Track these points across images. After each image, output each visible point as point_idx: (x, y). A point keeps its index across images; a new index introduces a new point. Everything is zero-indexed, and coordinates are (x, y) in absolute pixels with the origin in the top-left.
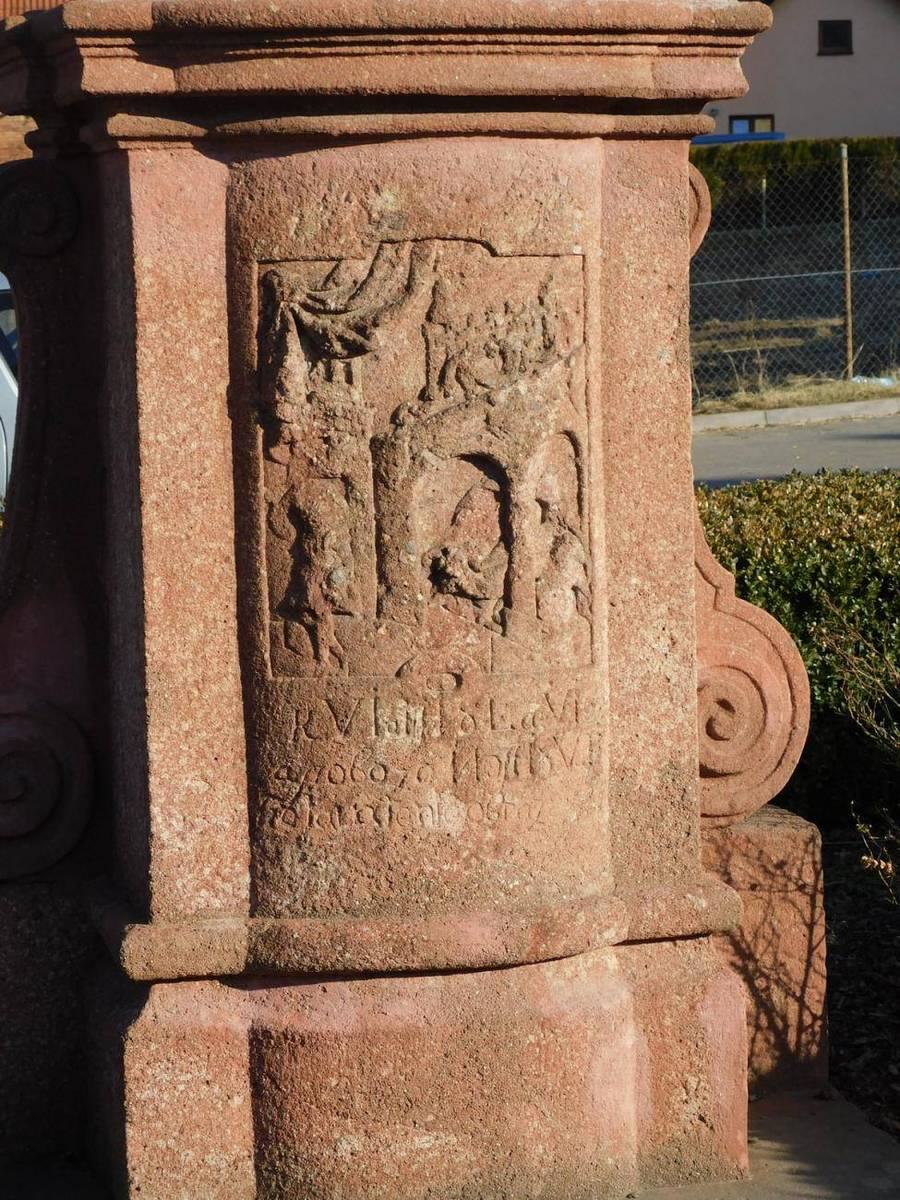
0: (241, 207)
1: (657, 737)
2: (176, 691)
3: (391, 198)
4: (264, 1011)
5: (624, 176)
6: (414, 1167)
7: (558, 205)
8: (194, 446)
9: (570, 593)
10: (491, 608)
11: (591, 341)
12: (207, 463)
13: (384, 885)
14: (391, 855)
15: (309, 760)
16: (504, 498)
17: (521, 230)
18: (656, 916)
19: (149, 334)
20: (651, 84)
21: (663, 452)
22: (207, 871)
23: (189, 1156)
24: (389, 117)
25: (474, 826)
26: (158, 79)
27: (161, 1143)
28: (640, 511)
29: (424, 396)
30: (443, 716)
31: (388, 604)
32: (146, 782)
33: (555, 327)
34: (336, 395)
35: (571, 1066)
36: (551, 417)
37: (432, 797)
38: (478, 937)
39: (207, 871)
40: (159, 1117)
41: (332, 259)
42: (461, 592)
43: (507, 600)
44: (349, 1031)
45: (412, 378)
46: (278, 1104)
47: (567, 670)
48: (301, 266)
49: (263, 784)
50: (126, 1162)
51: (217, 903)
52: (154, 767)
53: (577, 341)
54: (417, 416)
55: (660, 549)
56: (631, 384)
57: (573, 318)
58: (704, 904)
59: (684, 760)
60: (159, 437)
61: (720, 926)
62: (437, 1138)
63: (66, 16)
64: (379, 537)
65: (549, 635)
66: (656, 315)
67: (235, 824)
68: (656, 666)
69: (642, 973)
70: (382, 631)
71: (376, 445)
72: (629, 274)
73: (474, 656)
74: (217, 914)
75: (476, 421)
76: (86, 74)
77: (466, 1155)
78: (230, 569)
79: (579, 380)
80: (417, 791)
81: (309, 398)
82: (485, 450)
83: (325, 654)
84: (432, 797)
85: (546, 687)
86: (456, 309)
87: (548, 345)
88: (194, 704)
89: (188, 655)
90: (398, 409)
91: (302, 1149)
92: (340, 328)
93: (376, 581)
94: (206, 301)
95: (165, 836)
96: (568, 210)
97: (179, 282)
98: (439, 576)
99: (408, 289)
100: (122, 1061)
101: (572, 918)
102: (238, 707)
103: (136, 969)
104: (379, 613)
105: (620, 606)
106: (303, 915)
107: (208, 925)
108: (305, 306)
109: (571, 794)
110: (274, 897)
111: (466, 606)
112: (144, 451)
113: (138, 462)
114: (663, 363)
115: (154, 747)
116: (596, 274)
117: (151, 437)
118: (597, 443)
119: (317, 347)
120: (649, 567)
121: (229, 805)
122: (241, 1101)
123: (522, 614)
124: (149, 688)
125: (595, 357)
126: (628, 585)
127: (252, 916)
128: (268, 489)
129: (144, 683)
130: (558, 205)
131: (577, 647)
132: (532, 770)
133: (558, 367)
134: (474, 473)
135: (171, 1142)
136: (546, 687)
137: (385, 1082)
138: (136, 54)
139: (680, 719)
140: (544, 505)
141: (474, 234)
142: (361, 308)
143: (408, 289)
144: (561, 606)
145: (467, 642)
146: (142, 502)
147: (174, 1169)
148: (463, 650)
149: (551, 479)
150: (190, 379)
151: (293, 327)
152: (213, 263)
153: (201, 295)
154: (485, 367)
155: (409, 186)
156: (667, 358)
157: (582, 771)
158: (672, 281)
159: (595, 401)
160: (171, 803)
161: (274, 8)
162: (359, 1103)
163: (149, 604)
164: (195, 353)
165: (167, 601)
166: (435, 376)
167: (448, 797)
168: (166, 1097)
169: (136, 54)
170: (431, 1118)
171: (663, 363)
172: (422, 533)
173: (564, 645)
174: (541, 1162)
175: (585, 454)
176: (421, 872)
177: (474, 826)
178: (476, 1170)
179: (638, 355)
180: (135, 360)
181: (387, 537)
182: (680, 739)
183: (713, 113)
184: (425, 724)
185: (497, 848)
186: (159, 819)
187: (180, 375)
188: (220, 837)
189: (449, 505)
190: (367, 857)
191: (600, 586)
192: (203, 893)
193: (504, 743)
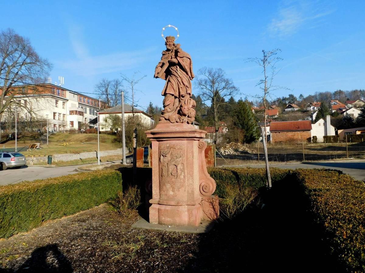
10: (176, 177)
18: (189, 203)
29: (171, 160)
37: (170, 191)
38: (173, 203)
45: (170, 159)
77: (172, 221)
84: (170, 191)
86: (173, 154)
99: (169, 152)
116: (186, 151)
121: (158, 191)
122: (157, 214)
123: (178, 177)
128: (160, 167)
142: (166, 153)
143: (169, 152)
145: (173, 179)
146: (335, 92)
152: (158, 150)
164: (156, 156)
165: (154, 175)
172: (170, 170)
173: (182, 180)
189: (173, 169)
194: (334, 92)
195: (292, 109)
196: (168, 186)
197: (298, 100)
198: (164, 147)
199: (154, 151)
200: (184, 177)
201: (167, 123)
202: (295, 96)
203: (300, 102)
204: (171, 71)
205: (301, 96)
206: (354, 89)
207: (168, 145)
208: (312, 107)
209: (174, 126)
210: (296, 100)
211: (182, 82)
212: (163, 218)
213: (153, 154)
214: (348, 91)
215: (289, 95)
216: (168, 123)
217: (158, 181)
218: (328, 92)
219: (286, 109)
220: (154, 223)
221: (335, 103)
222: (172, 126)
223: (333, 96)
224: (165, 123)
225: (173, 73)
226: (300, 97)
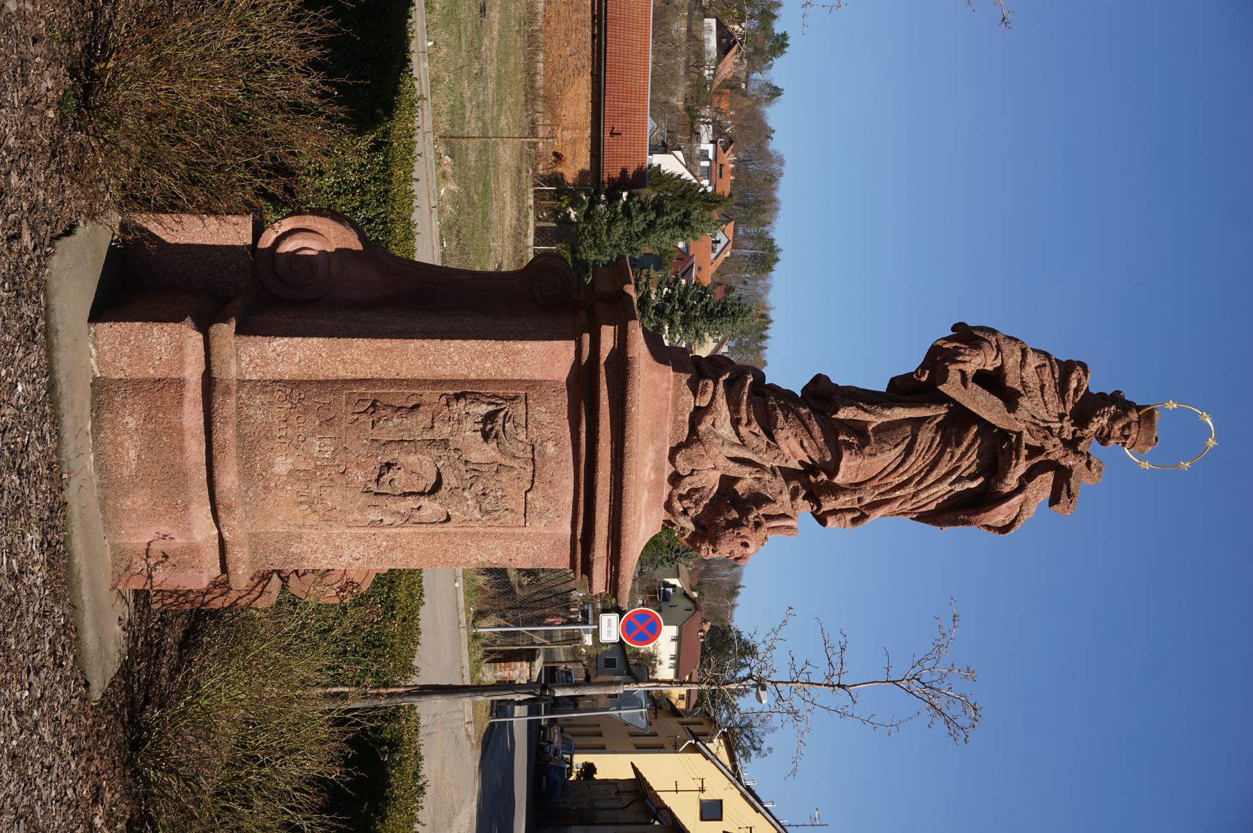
0: (549, 387)
1: (315, 552)
2: (340, 350)
3: (552, 450)
4: (194, 384)
5: (558, 543)
6: (120, 450)
7: (547, 517)
8: (448, 363)
9: (380, 518)
10: (374, 487)
11: (489, 528)
12: (440, 368)
13: (251, 439)
14: (264, 442)
15: (306, 409)
16: (422, 494)
17: (537, 503)
19: (498, 346)
20: (596, 556)
22: (258, 361)
23: (126, 349)
24: (584, 452)
25: (277, 478)
26: (604, 354)
27: (132, 338)
28: (415, 547)
29: (466, 462)
30: (326, 466)
31: (376, 444)
32: (298, 336)
33: (496, 515)
34: (468, 425)
35: (167, 517)
36: (457, 513)
37: (290, 460)
38: (228, 479)
39: (258, 361)
40: (144, 337)
41: (527, 425)
42: (381, 475)
43: (376, 494)
44: (184, 423)
45: (475, 457)
46: (152, 561)
47: (345, 517)
48: (524, 411)
49: (298, 387)
50: (124, 321)
51: (243, 364)
52: (306, 340)
53: (488, 523)
54: (459, 459)
55: (398, 555)
56: (470, 544)
57: (499, 522)
58: (240, 573)
59: (305, 563)
60: (452, 349)
61: (231, 579)
62: (134, 460)
63: (633, 321)
64: (406, 441)
65: (361, 510)
66: (499, 554)
67: (279, 374)
69: (209, 545)
70: (365, 441)
71: (445, 442)
72: (517, 544)
73: (353, 480)
74: (239, 363)
75: (454, 483)
76: (608, 327)
77: (126, 473)
78: (393, 375)
79: (471, 524)
80: (293, 454)
81: (467, 413)
82: (443, 486)
83: (356, 417)
84: (290, 460)
85: (338, 508)
87: (488, 512)
88: (333, 358)
89: (356, 357)
90: (924, 518)
91: (129, 401)
92: (497, 428)
93: (387, 439)
94: (510, 370)
95: (274, 344)
96: (545, 521)
97: (519, 359)
98: (389, 466)
99: (514, 456)
100: (171, 321)
101: (234, 519)
102: (332, 377)
103: (216, 329)
104: (373, 440)
105: (373, 538)
106: (237, 402)
107: (233, 361)
108: (507, 413)
109: (290, 517)
110: (245, 390)
111: (375, 476)
112: (446, 342)
113: (442, 338)
114: (479, 557)
115: (315, 340)
117: (452, 345)
118: (445, 529)
119: (490, 417)
120: (391, 550)
121: (288, 371)
123: (373, 500)
124: (341, 339)
125: (482, 530)
126: (383, 541)
127: (237, 380)
128: (429, 395)
129: (344, 336)
130: (547, 517)
131: (356, 521)
132: (301, 502)
133: (478, 516)
134: (433, 479)
135: (133, 342)
136: (338, 508)
137: (160, 439)
138: (584, 361)
139: (323, 561)
140: (419, 508)
141: (536, 484)
144: (374, 515)
145: (359, 476)
147: (120, 344)
148: (356, 475)
149: (429, 511)
150: (477, 362)
151: (498, 408)
152: (526, 373)
153: (512, 368)
154: (479, 487)
155: (557, 458)
156: (481, 559)
157: (300, 523)
158: (513, 561)
159: (463, 529)
160: (289, 347)
161: (633, 409)
162: (150, 426)
163: (379, 341)
164: (488, 365)
166: (475, 467)
167: (290, 467)
168: (154, 341)
169: (584, 361)
170: (143, 457)
171: (479, 557)
173: (356, 515)
174: (122, 504)
175: (440, 525)
176: (256, 455)
177: (277, 478)
178: (119, 476)
179: (482, 547)
180: (486, 339)
181: (406, 444)
182: (314, 562)
183: (652, 633)
184: (323, 458)
185: (265, 487)
186: (282, 341)
187: (479, 358)
188: (273, 367)
190: (263, 432)
191: (383, 530)
192: (248, 359)
193: (314, 491)
194: (773, 235)
195: (714, 55)
196: (320, 447)
197: (756, 76)
198: (540, 425)
199: (519, 352)
200: (372, 524)
202: (779, 63)
203: (743, 86)
204: (959, 444)
205: (776, 92)
206: (772, 315)
207: (551, 449)
208: (710, 148)
209: (658, 469)
210: (753, 68)
212: (132, 422)
214: (767, 293)
215: (784, 36)
216: (675, 430)
217: (342, 374)
218: (777, 209)
219: (712, 22)
220: (94, 352)
221: (719, 247)
222: (659, 452)
223: (752, 231)
224: (677, 411)
225: (947, 457)
226: (768, 85)
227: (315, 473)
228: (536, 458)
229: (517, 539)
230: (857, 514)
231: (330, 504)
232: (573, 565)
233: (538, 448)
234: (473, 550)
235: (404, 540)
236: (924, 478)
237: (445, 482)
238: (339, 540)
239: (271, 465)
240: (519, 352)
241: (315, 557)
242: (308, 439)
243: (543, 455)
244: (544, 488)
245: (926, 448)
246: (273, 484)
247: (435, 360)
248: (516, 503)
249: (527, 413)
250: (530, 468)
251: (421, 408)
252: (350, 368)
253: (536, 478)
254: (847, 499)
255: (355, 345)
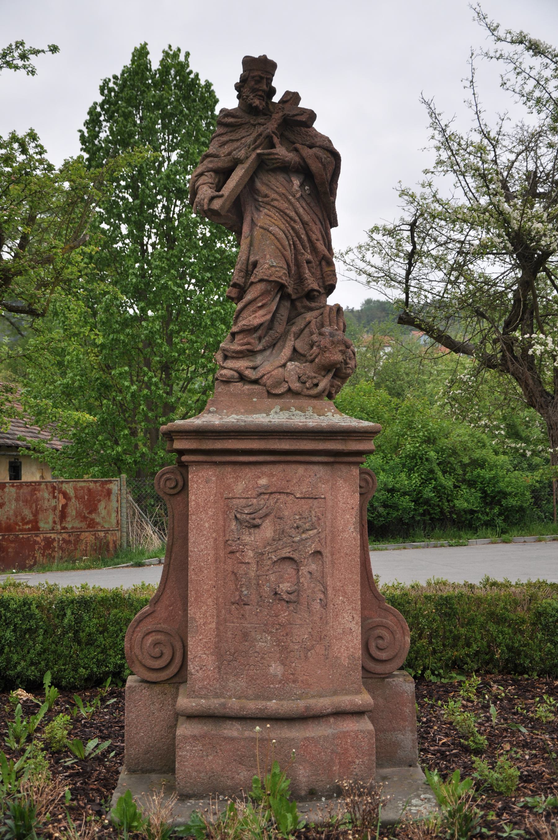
2: (197, 626)
17: (304, 490)
21: (350, 558)
55: (349, 589)
68: (348, 625)
72: (340, 504)
85: (310, 630)
111: (285, 604)
112: (190, 553)
120: (346, 593)
131: (321, 618)
136: (310, 630)
141: (289, 491)
150: (205, 532)
154: (293, 532)
156: (352, 530)
159: (328, 542)
164: (207, 525)
182: (355, 649)
187: (201, 531)
198: (246, 490)
199: (197, 504)
201: (251, 395)
211: (310, 240)
213: (194, 517)
227: (282, 646)
228: (269, 491)
229: (337, 504)
230: (324, 263)
231: (306, 636)
232: (357, 464)
233: (263, 490)
234: (346, 535)
235: (338, 584)
236: (291, 218)
237: (288, 555)
238: (338, 630)
239: (276, 676)
240: (197, 504)
241: (352, 648)
242: (257, 650)
243: (267, 487)
244: (292, 486)
245: (270, 218)
246: (291, 676)
247: (204, 561)
248: (304, 505)
249: (239, 498)
250: (277, 496)
251: (235, 571)
252: (210, 619)
253: (285, 491)
254: (307, 271)
255: (193, 616)
